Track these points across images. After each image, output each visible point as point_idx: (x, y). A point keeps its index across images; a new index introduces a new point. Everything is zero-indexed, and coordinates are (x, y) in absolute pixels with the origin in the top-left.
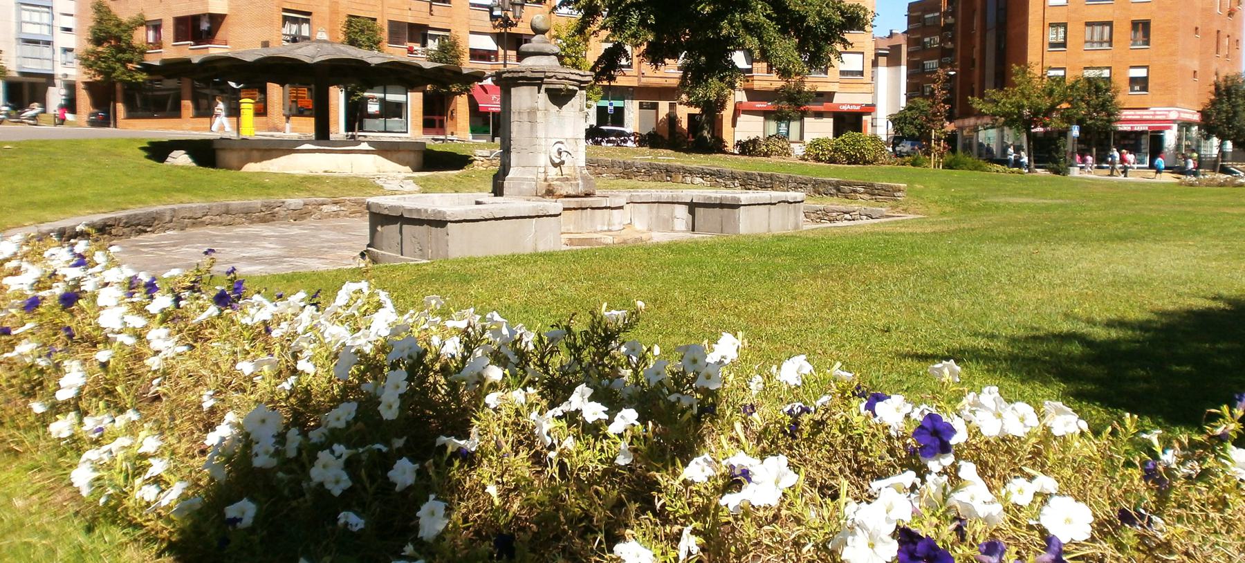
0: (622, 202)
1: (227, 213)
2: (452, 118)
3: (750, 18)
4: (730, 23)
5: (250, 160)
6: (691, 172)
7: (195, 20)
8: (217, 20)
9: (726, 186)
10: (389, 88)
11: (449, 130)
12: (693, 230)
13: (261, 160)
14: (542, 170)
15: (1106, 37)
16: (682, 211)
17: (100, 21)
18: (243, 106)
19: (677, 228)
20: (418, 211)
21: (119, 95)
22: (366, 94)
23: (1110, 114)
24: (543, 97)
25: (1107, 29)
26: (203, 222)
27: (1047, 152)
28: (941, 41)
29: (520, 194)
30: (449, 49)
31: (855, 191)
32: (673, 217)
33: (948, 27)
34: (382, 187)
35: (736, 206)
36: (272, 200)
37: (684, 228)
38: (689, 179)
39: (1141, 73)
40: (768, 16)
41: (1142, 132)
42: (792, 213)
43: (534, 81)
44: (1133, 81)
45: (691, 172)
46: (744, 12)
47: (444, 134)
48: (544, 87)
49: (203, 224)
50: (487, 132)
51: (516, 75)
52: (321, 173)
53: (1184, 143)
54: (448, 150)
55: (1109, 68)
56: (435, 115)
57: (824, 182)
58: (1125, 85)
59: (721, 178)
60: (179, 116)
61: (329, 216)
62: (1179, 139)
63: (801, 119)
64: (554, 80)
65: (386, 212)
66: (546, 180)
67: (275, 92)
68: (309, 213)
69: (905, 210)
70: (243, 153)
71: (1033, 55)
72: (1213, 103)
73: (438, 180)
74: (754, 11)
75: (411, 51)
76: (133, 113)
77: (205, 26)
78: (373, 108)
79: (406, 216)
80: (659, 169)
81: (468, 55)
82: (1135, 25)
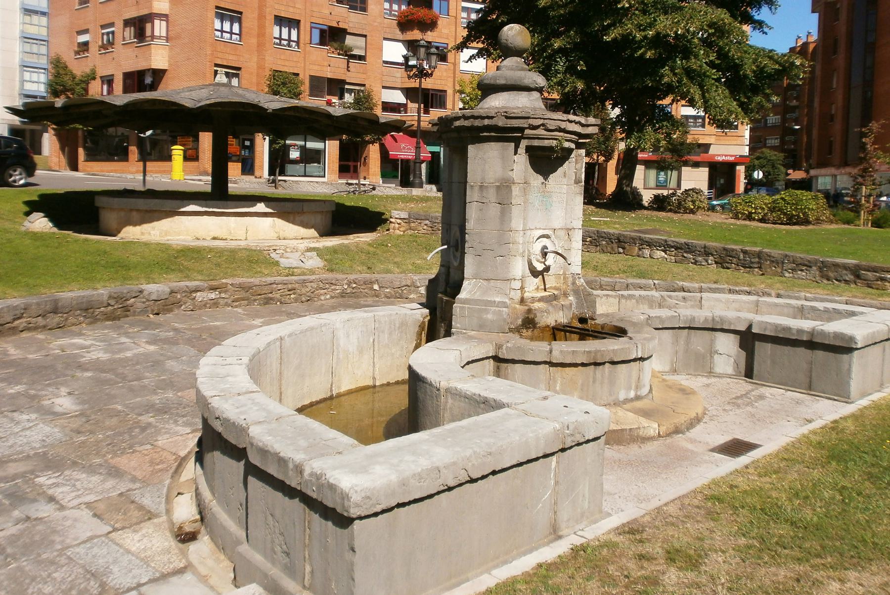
1: (55, 311)
2: (365, 164)
3: (694, 64)
4: (672, 70)
7: (141, 74)
8: (158, 75)
10: (309, 137)
11: (362, 175)
12: (749, 373)
14: (517, 285)
16: (727, 345)
17: (57, 75)
18: (174, 152)
19: (718, 369)
20: (282, 462)
21: (81, 141)
22: (288, 142)
24: (521, 162)
30: (363, 99)
32: (712, 352)
34: (277, 263)
35: (849, 350)
37: (730, 370)
38: (647, 252)
40: (712, 65)
43: (506, 133)
45: (650, 244)
46: (686, 57)
47: (357, 178)
48: (524, 144)
50: (397, 177)
51: (477, 123)
54: (360, 204)
56: (350, 163)
57: (836, 265)
59: (690, 252)
60: (127, 160)
64: (541, 132)
66: (522, 301)
68: (178, 304)
70: (122, 214)
75: (329, 103)
76: (92, 156)
77: (148, 80)
78: (294, 154)
80: (609, 238)
81: (380, 107)
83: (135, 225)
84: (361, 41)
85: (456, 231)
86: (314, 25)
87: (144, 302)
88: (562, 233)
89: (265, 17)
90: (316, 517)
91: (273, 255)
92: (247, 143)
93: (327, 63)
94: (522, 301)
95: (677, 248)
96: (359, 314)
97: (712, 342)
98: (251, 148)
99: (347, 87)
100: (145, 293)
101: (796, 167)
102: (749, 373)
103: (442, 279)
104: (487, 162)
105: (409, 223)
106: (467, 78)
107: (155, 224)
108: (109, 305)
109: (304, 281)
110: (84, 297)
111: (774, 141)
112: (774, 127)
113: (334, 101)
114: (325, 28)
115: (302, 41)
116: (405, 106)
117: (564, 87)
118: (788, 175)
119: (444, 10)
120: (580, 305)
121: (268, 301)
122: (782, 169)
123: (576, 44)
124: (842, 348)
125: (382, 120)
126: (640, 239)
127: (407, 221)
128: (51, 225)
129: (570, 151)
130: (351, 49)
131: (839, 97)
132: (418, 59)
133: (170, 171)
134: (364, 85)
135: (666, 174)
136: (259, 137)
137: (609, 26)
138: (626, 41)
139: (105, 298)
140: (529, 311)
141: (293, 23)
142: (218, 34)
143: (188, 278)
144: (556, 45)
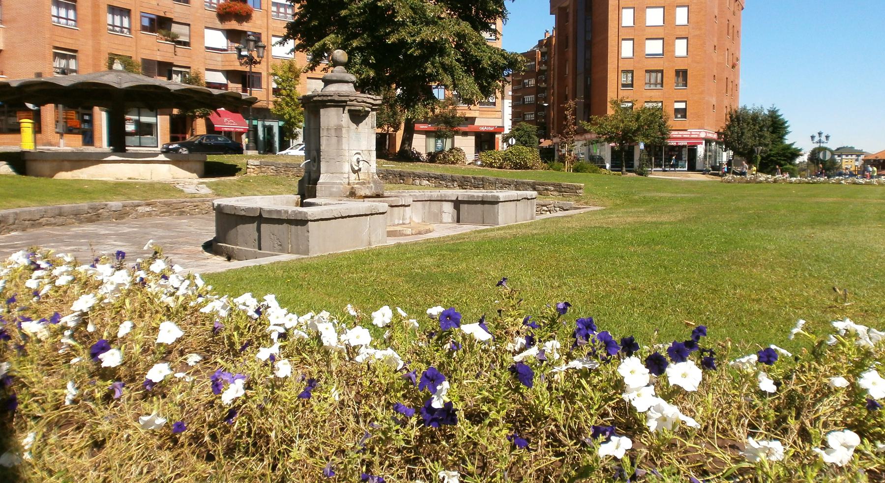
0: (409, 201)
3: (447, 60)
4: (433, 64)
5: (61, 169)
6: (419, 176)
9: (447, 187)
10: (143, 111)
12: (458, 221)
13: (71, 169)
14: (346, 176)
15: (659, 81)
16: (448, 208)
18: (23, 125)
19: (444, 221)
23: (663, 134)
24: (346, 117)
25: (660, 75)
26: (40, 223)
27: (623, 160)
28: (537, 82)
29: (331, 195)
31: (547, 190)
32: (441, 212)
33: (541, 72)
34: (182, 191)
35: (497, 203)
36: (96, 203)
37: (450, 220)
38: (418, 182)
39: (682, 106)
40: (458, 60)
41: (684, 146)
42: (529, 208)
43: (338, 103)
44: (677, 111)
45: (419, 176)
48: (347, 108)
49: (41, 225)
51: (325, 98)
52: (125, 180)
53: (708, 154)
55: (662, 102)
58: (672, 113)
61: (143, 215)
62: (706, 151)
63: (452, 137)
64: (355, 103)
65: (243, 213)
66: (349, 184)
67: (49, 112)
68: (127, 214)
69: (586, 203)
70: (55, 164)
71: (611, 95)
72: (729, 127)
73: (225, 184)
74: (449, 55)
79: (265, 215)
80: (394, 174)
82: (678, 72)
83: (67, 171)
84: (185, 30)
85: (314, 153)
88: (366, 152)
89: (99, 6)
90: (293, 227)
91: (178, 186)
92: (87, 118)
93: (155, 48)
94: (349, 184)
95: (435, 178)
97: (441, 206)
98: (90, 122)
99: (174, 69)
101: (547, 137)
102: (458, 221)
103: (306, 179)
104: (330, 117)
106: (278, 63)
107: (84, 169)
109: (203, 201)
111: (530, 116)
112: (530, 104)
115: (133, 28)
117: (361, 75)
118: (540, 143)
119: (257, 5)
120: (376, 188)
121: (182, 213)
122: (537, 139)
123: (367, 44)
124: (495, 202)
125: (243, 98)
126: (413, 173)
127: (259, 167)
128: (11, 170)
129: (368, 112)
131: (570, 81)
132: (248, 50)
133: (20, 140)
134: (189, 68)
135: (442, 142)
136: (96, 109)
137: (390, 32)
138: (402, 43)
140: (353, 188)
141: (125, 12)
142: (55, 19)
143: (130, 198)
144: (354, 45)
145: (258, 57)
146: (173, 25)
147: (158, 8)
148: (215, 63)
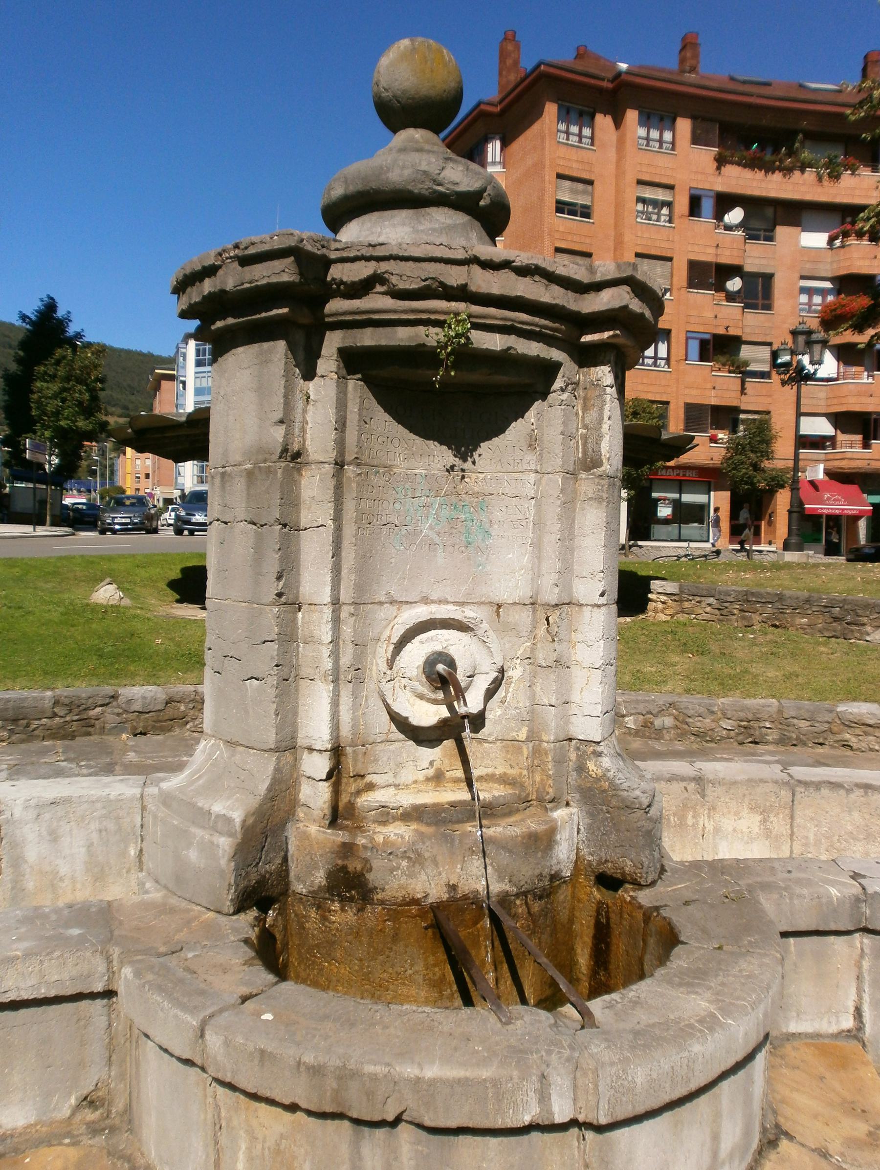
22: (655, 495)
48: (333, 342)
50: (818, 540)
78: (664, 511)
86: (689, 335)
87: (118, 715)
96: (83, 787)
100: (121, 700)
105: (681, 601)
108: (55, 715)
110: (8, 701)
113: (720, 436)
114: (707, 337)
116: (832, 439)
130: (746, 364)
139: (48, 704)
145: (812, 363)
146: (744, 347)
147: (715, 322)
148: (815, 402)
